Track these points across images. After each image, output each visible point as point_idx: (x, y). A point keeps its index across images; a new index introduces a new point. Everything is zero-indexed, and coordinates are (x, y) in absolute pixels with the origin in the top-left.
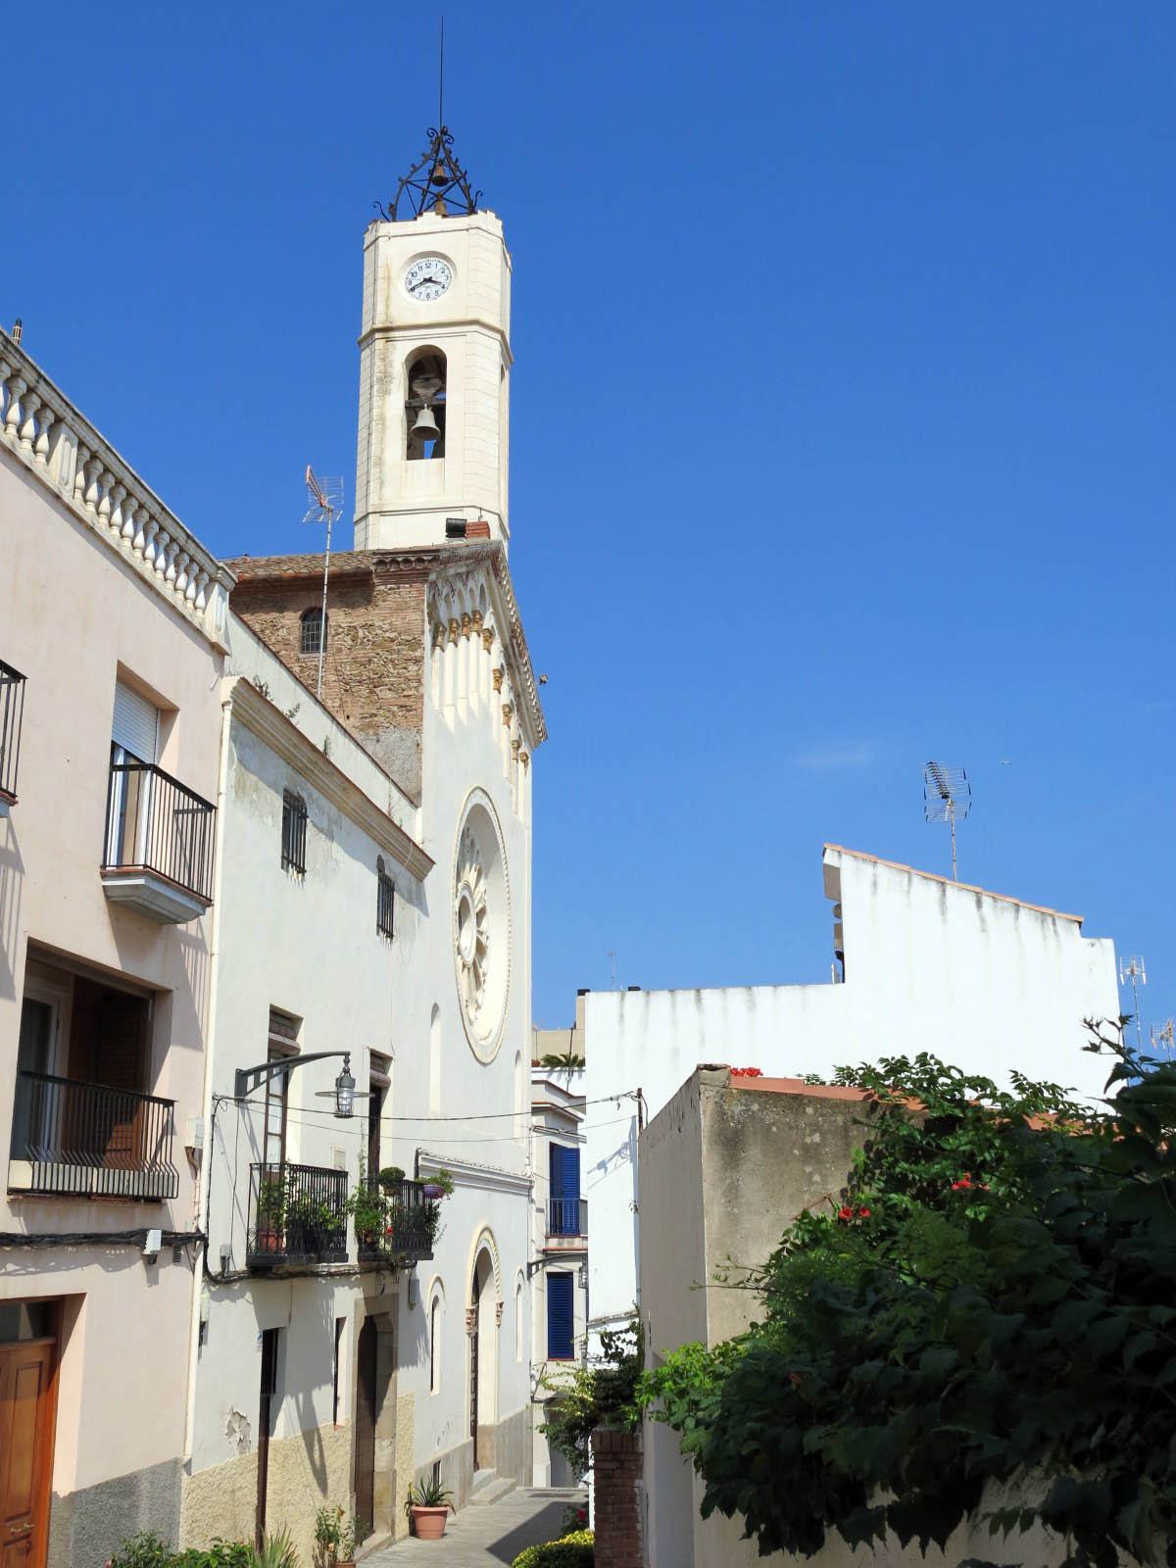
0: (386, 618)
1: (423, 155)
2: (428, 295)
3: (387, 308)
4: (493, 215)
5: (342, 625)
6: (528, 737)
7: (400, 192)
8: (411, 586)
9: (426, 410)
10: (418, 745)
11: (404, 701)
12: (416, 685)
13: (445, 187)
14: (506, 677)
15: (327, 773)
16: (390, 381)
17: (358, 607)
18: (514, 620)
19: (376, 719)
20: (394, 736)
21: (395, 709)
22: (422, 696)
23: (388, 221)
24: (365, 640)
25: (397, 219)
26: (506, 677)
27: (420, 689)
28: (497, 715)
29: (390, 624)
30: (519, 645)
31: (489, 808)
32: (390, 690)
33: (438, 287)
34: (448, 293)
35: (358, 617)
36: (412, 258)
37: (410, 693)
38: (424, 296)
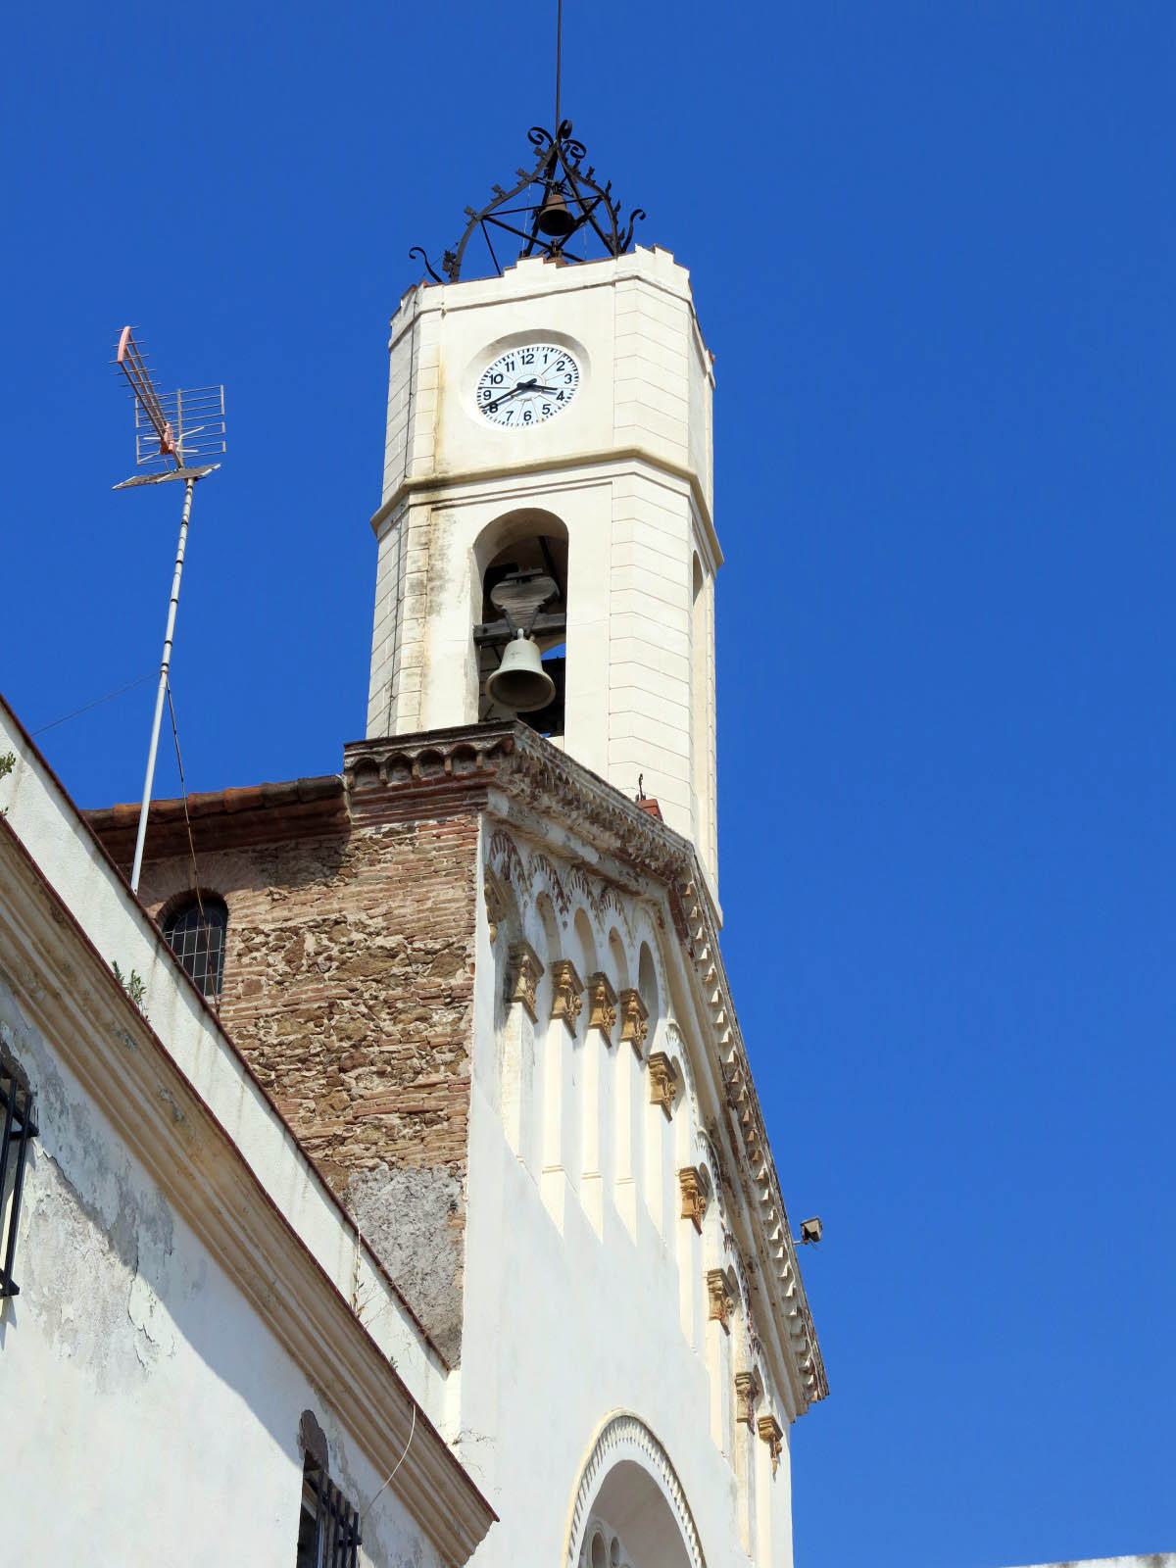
0: (375, 903)
1: (520, 173)
2: (527, 416)
3: (437, 443)
4: (670, 257)
5: (266, 928)
6: (779, 1384)
7: (468, 233)
8: (442, 824)
9: (522, 640)
10: (453, 1207)
11: (418, 1099)
12: (449, 1057)
13: (567, 222)
14: (714, 1207)
15: (108, 1028)
16: (441, 587)
17: (306, 881)
18: (731, 1059)
19: (342, 1149)
20: (389, 1188)
21: (394, 1120)
22: (467, 1083)
23: (439, 281)
24: (320, 959)
25: (462, 271)
26: (714, 1207)
27: (461, 1068)
28: (694, 1299)
29: (386, 915)
30: (745, 1126)
31: (657, 1470)
32: (381, 1074)
33: (551, 398)
34: (570, 408)
35: (306, 905)
36: (498, 342)
37: (434, 1078)
38: (517, 417)
